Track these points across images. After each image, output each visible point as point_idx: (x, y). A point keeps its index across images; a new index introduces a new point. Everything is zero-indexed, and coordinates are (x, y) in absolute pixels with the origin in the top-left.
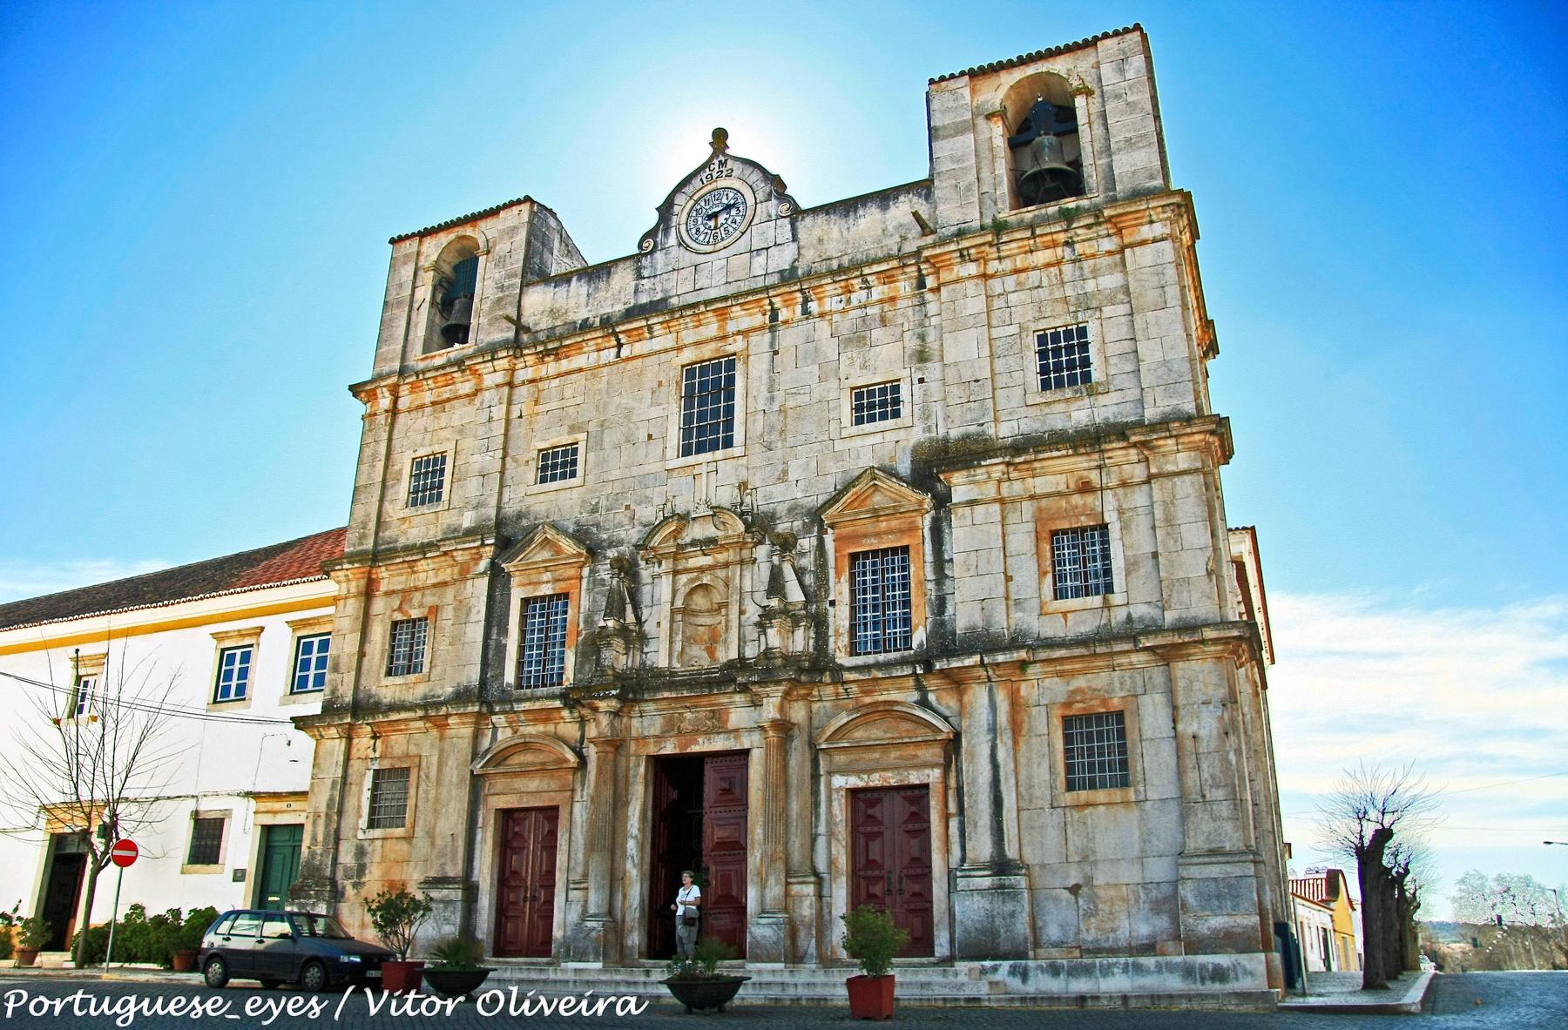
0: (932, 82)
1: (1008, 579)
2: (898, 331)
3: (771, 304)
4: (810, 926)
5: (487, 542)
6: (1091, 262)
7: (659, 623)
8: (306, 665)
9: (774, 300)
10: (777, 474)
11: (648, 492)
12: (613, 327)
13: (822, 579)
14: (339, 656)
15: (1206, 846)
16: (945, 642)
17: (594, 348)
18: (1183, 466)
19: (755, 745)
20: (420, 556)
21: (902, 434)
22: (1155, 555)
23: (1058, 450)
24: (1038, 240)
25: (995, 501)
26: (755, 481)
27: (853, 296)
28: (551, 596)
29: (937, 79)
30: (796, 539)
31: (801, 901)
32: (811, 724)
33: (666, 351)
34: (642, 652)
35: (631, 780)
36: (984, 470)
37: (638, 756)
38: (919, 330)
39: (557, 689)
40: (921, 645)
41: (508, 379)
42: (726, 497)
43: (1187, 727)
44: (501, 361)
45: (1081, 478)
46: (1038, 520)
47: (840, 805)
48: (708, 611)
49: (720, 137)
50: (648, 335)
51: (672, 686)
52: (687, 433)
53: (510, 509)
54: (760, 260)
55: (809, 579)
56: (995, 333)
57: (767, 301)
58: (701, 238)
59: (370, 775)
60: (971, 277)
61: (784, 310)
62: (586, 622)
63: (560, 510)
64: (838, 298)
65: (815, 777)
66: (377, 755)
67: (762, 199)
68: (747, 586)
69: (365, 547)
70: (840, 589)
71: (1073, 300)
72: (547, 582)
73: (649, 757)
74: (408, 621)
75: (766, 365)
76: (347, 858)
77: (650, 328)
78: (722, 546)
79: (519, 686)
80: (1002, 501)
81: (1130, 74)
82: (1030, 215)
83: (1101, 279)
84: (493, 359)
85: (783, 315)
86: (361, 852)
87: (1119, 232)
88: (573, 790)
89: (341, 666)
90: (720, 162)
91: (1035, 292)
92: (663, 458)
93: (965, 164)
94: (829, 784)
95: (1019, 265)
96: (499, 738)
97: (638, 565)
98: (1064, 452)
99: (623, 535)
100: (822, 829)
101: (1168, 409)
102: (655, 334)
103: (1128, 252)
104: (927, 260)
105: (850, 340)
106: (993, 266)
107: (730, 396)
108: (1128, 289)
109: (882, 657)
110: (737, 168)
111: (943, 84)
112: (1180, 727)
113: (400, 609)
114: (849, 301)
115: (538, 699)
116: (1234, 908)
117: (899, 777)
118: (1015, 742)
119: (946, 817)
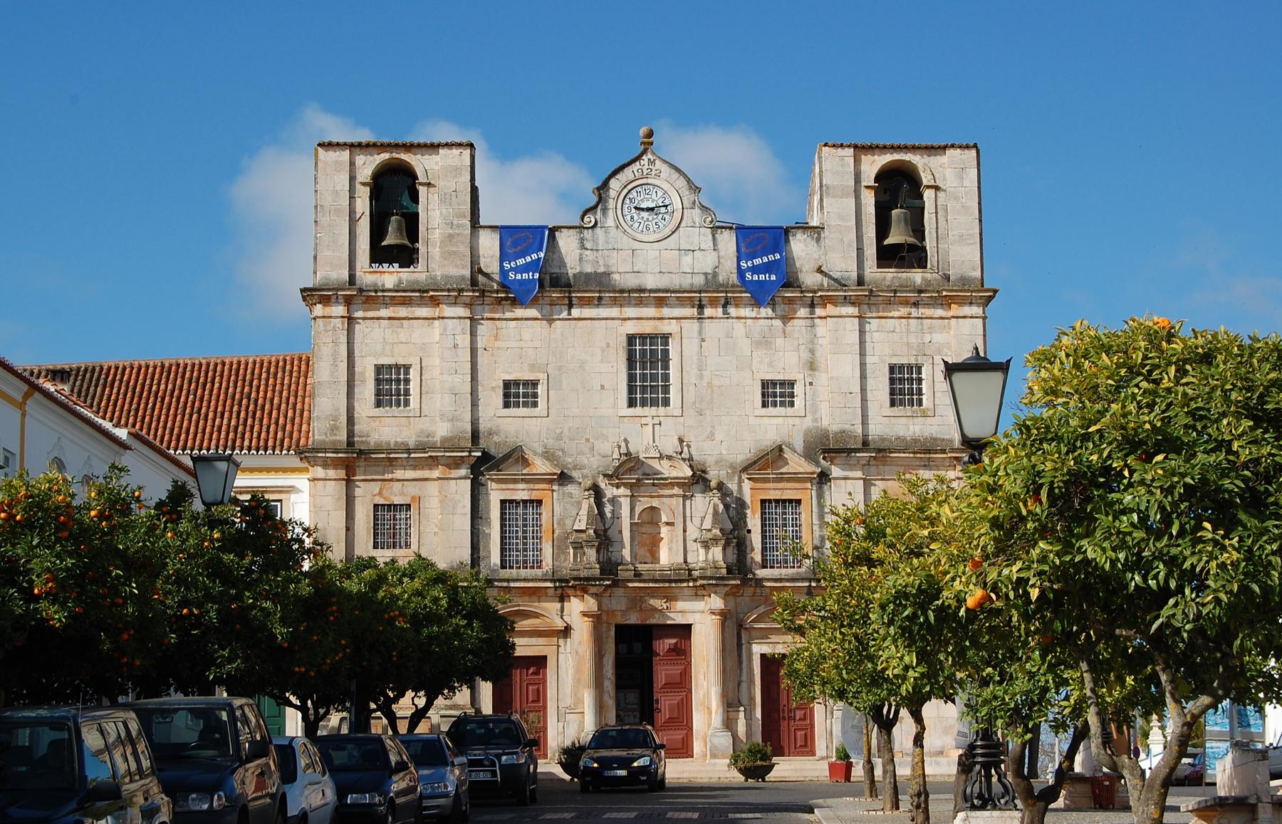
2: (796, 343)
9: (703, 299)
10: (706, 434)
11: (605, 431)
12: (570, 292)
17: (548, 302)
34: (608, 550)
37: (609, 624)
38: (810, 346)
54: (687, 259)
65: (739, 645)
69: (338, 438)
73: (617, 626)
75: (696, 349)
81: (966, 183)
83: (934, 335)
92: (615, 406)
100: (744, 678)
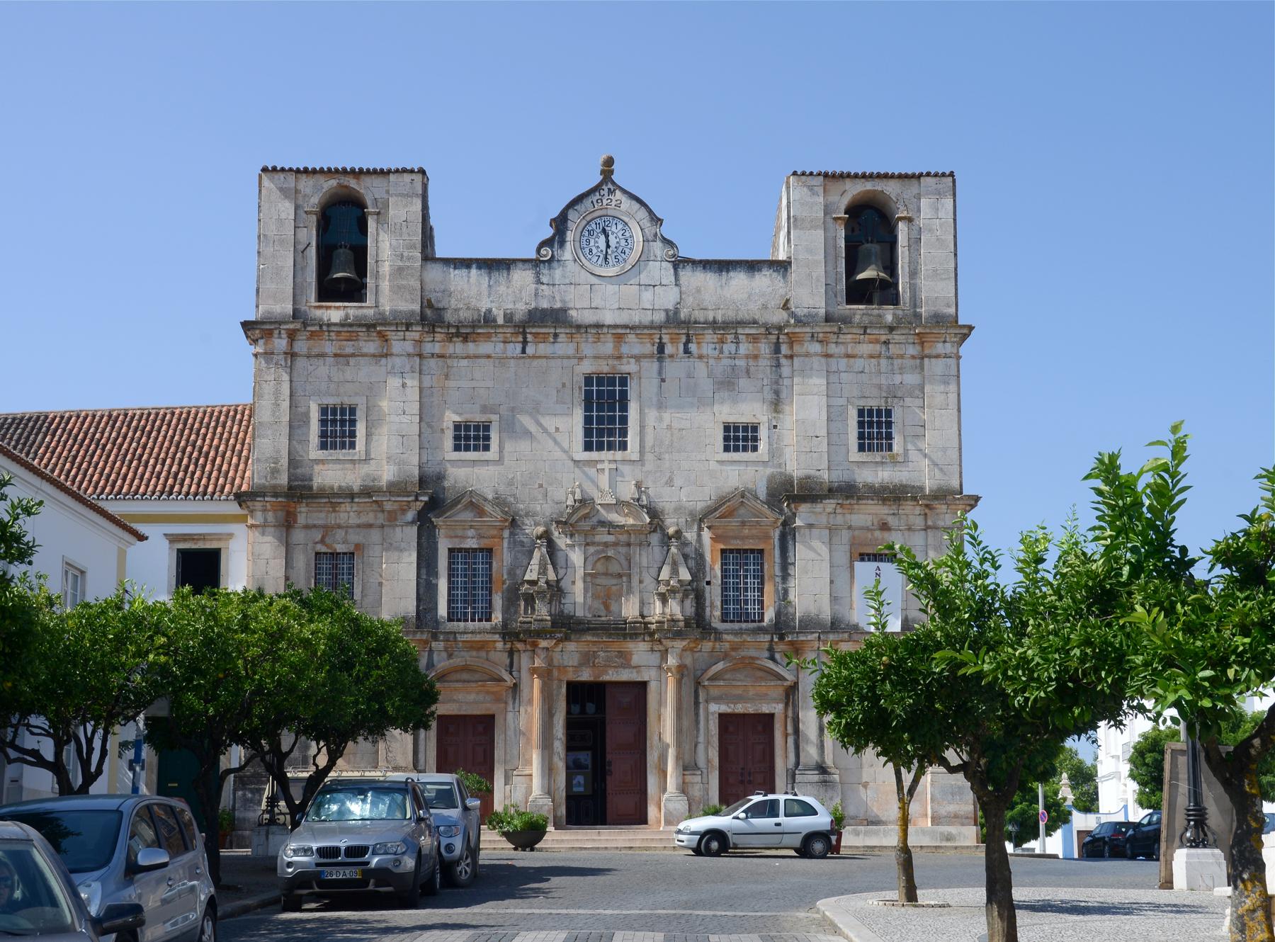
3: (660, 338)
4: (700, 803)
6: (900, 361)
9: (663, 336)
25: (826, 528)
27: (725, 346)
28: (475, 550)
33: (569, 358)
34: (560, 602)
40: (771, 620)
41: (418, 349)
44: (414, 334)
48: (603, 574)
50: (552, 340)
60: (816, 354)
62: (509, 573)
64: (713, 346)
65: (697, 703)
68: (645, 563)
69: (278, 482)
71: (885, 388)
75: (655, 390)
77: (556, 335)
84: (407, 330)
85: (669, 349)
87: (922, 343)
88: (506, 703)
90: (609, 189)
94: (707, 709)
95: (850, 351)
100: (701, 739)
103: (926, 360)
105: (722, 383)
106: (832, 349)
107: (624, 408)
109: (736, 626)
113: (322, 541)
114: (721, 352)
116: (961, 799)
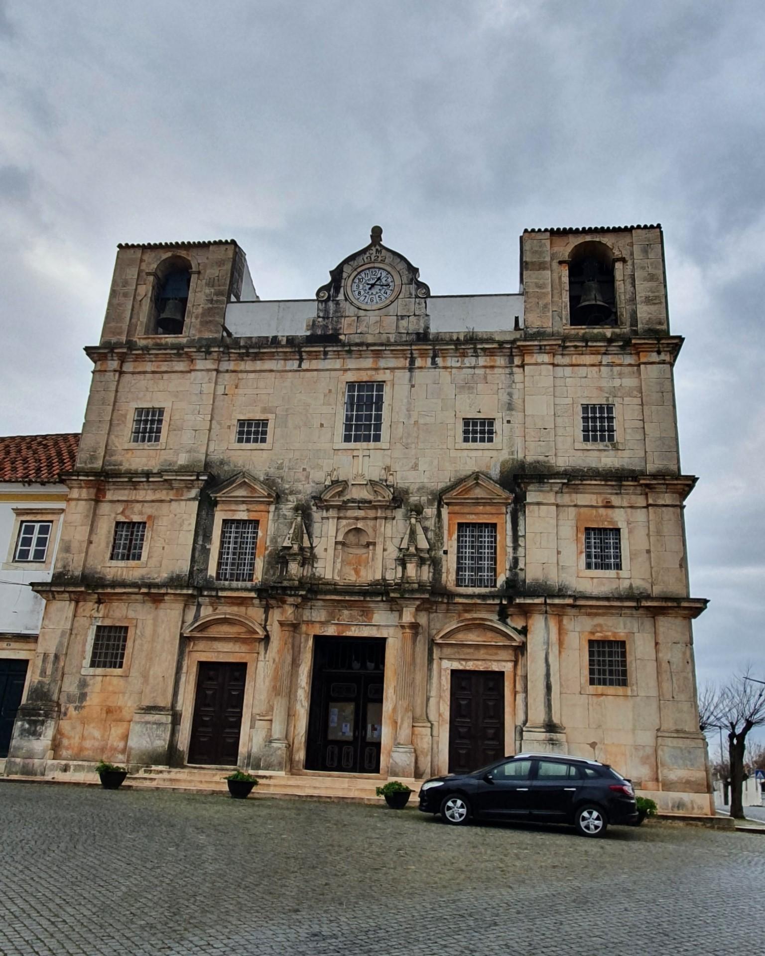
0: (526, 231)
1: (559, 553)
2: (495, 387)
3: (412, 354)
5: (201, 478)
6: (618, 368)
7: (326, 550)
8: (27, 542)
9: (414, 352)
10: (411, 465)
11: (320, 462)
13: (439, 535)
14: (70, 541)
15: (674, 728)
16: (515, 587)
18: (668, 502)
19: (391, 635)
20: (144, 479)
21: (494, 454)
22: (648, 552)
23: (596, 480)
24: (588, 349)
25: (553, 504)
26: (396, 467)
29: (529, 230)
30: (423, 509)
31: (422, 739)
32: (429, 626)
34: (313, 567)
35: (302, 650)
36: (549, 485)
39: (249, 584)
40: (502, 586)
42: (376, 474)
43: (665, 655)
45: (606, 499)
46: (578, 519)
47: (446, 678)
49: (377, 233)
51: (336, 592)
52: (348, 428)
53: (215, 457)
55: (431, 535)
56: (558, 401)
57: (409, 352)
58: (362, 298)
59: (94, 629)
61: (419, 359)
62: (271, 541)
63: (253, 463)
66: (100, 615)
67: (406, 282)
69: (95, 466)
70: (451, 544)
72: (244, 511)
74: (129, 523)
76: (70, 686)
78: (375, 506)
79: (218, 578)
80: (557, 506)
82: (583, 331)
86: (83, 684)
87: (638, 354)
89: (72, 548)
90: (377, 250)
91: (583, 380)
92: (332, 441)
93: (543, 291)
94: (440, 665)
95: (574, 362)
96: (202, 614)
97: (311, 509)
98: (598, 482)
99: (300, 487)
101: (661, 466)
102: (328, 357)
103: (642, 366)
104: (518, 347)
105: (463, 387)
107: (379, 408)
108: (641, 389)
110: (389, 258)
111: (533, 234)
112: (660, 655)
115: (237, 589)
117: (485, 666)
118: (560, 652)
119: (515, 693)
